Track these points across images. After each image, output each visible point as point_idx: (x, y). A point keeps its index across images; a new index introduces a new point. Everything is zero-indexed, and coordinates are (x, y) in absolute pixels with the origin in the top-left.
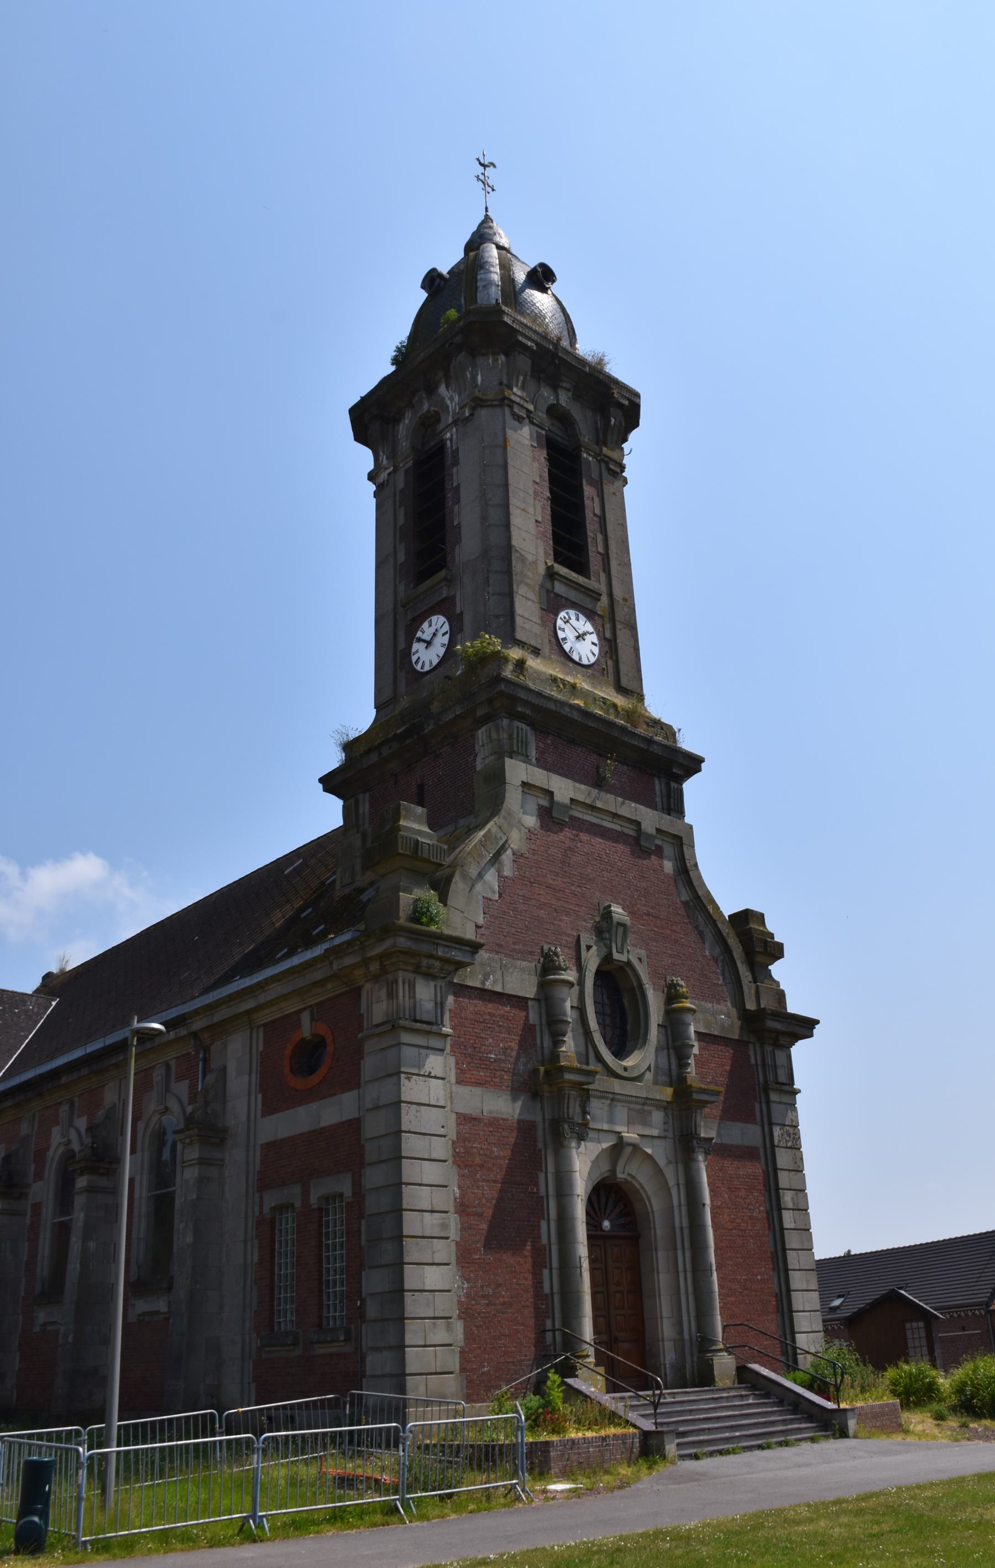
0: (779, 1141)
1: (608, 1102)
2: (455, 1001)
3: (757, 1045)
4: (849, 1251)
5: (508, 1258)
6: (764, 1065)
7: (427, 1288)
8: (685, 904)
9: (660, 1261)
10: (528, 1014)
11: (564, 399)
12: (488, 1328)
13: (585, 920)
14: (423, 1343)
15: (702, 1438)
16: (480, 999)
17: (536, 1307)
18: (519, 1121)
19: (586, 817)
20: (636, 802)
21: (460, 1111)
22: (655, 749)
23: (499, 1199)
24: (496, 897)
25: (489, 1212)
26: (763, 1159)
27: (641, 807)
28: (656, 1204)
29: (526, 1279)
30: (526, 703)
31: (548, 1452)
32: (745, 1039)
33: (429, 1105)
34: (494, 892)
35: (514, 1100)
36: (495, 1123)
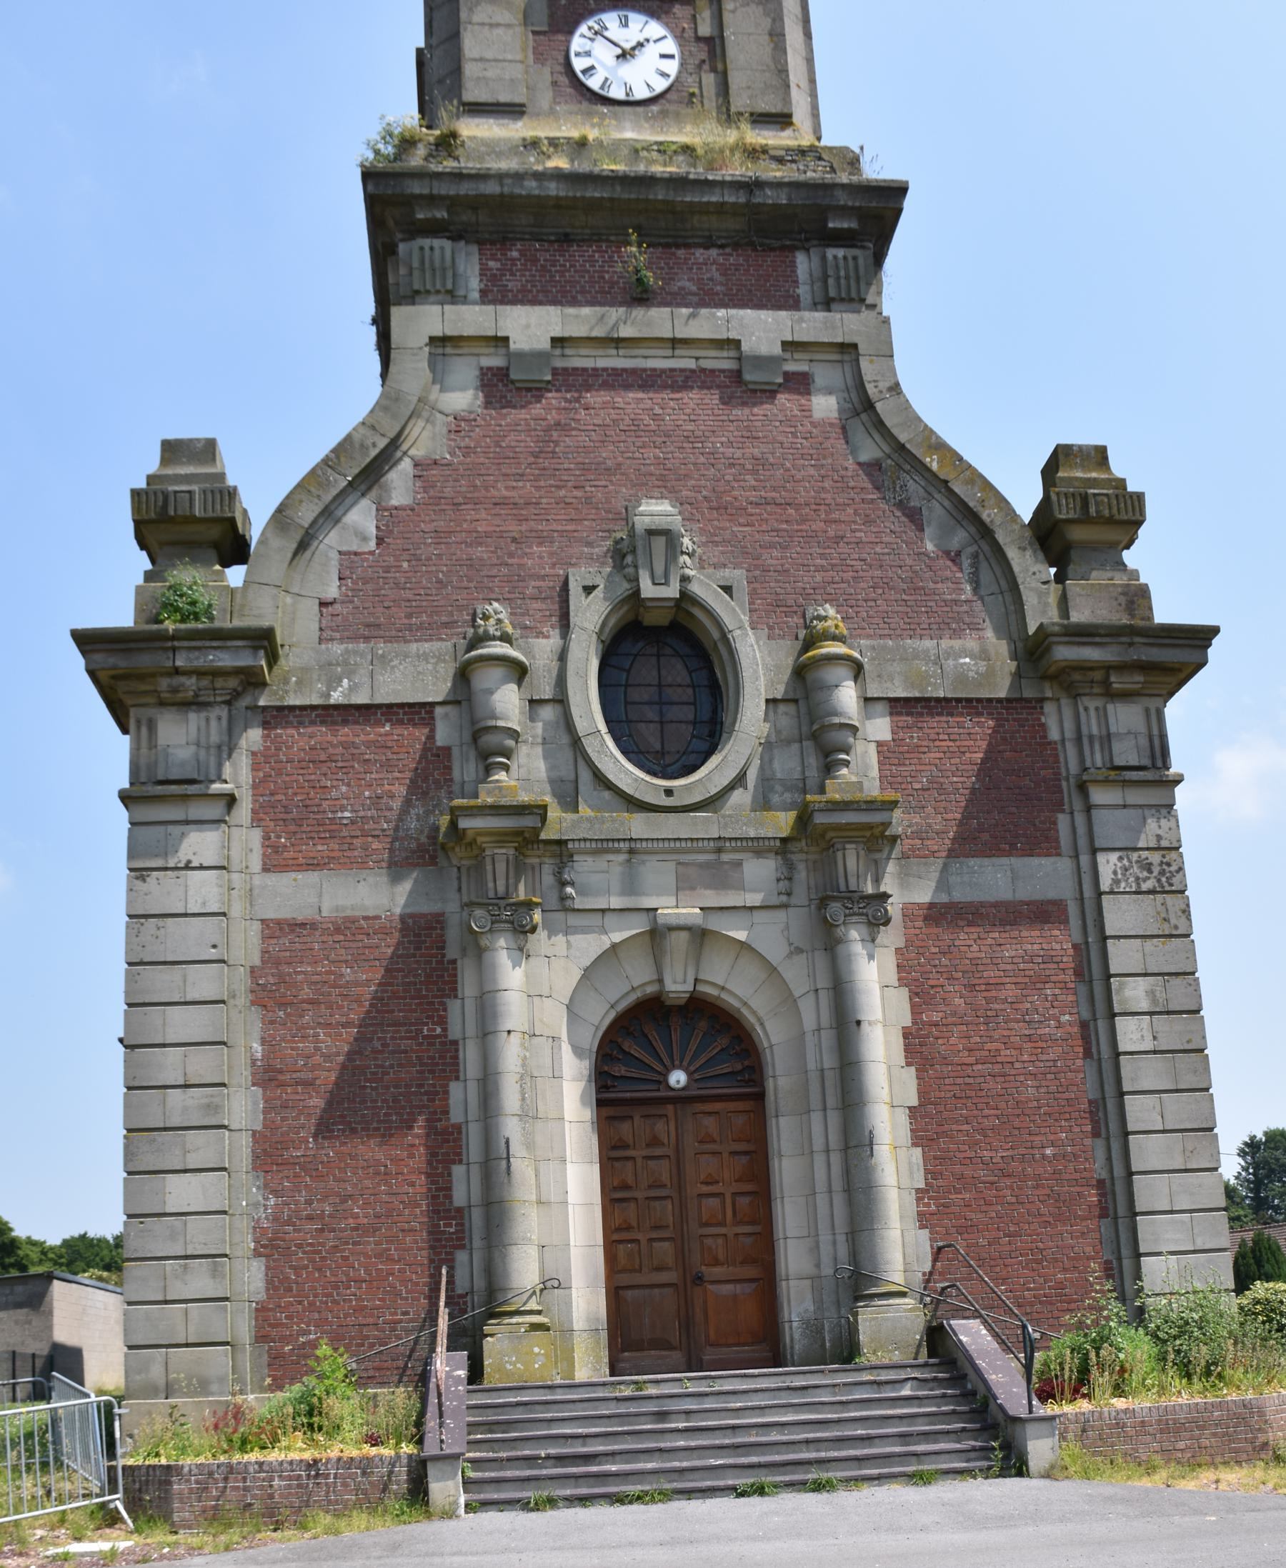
0: (1116, 882)
1: (622, 857)
2: (265, 737)
3: (1065, 702)
5: (371, 1150)
6: (1079, 739)
7: (168, 1210)
8: (872, 468)
9: (784, 1136)
10: (433, 731)
12: (320, 1270)
13: (589, 544)
14: (161, 1298)
15: (677, 1464)
16: (323, 723)
18: (403, 918)
19: (601, 363)
20: (726, 306)
21: (270, 915)
22: (769, 197)
24: (372, 545)
25: (329, 1077)
26: (1075, 922)
27: (741, 312)
28: (773, 1034)
29: (412, 1184)
30: (432, 200)
31: (169, 1483)
32: (1028, 693)
33: (186, 915)
34: (365, 539)
35: (396, 879)
36: (346, 927)
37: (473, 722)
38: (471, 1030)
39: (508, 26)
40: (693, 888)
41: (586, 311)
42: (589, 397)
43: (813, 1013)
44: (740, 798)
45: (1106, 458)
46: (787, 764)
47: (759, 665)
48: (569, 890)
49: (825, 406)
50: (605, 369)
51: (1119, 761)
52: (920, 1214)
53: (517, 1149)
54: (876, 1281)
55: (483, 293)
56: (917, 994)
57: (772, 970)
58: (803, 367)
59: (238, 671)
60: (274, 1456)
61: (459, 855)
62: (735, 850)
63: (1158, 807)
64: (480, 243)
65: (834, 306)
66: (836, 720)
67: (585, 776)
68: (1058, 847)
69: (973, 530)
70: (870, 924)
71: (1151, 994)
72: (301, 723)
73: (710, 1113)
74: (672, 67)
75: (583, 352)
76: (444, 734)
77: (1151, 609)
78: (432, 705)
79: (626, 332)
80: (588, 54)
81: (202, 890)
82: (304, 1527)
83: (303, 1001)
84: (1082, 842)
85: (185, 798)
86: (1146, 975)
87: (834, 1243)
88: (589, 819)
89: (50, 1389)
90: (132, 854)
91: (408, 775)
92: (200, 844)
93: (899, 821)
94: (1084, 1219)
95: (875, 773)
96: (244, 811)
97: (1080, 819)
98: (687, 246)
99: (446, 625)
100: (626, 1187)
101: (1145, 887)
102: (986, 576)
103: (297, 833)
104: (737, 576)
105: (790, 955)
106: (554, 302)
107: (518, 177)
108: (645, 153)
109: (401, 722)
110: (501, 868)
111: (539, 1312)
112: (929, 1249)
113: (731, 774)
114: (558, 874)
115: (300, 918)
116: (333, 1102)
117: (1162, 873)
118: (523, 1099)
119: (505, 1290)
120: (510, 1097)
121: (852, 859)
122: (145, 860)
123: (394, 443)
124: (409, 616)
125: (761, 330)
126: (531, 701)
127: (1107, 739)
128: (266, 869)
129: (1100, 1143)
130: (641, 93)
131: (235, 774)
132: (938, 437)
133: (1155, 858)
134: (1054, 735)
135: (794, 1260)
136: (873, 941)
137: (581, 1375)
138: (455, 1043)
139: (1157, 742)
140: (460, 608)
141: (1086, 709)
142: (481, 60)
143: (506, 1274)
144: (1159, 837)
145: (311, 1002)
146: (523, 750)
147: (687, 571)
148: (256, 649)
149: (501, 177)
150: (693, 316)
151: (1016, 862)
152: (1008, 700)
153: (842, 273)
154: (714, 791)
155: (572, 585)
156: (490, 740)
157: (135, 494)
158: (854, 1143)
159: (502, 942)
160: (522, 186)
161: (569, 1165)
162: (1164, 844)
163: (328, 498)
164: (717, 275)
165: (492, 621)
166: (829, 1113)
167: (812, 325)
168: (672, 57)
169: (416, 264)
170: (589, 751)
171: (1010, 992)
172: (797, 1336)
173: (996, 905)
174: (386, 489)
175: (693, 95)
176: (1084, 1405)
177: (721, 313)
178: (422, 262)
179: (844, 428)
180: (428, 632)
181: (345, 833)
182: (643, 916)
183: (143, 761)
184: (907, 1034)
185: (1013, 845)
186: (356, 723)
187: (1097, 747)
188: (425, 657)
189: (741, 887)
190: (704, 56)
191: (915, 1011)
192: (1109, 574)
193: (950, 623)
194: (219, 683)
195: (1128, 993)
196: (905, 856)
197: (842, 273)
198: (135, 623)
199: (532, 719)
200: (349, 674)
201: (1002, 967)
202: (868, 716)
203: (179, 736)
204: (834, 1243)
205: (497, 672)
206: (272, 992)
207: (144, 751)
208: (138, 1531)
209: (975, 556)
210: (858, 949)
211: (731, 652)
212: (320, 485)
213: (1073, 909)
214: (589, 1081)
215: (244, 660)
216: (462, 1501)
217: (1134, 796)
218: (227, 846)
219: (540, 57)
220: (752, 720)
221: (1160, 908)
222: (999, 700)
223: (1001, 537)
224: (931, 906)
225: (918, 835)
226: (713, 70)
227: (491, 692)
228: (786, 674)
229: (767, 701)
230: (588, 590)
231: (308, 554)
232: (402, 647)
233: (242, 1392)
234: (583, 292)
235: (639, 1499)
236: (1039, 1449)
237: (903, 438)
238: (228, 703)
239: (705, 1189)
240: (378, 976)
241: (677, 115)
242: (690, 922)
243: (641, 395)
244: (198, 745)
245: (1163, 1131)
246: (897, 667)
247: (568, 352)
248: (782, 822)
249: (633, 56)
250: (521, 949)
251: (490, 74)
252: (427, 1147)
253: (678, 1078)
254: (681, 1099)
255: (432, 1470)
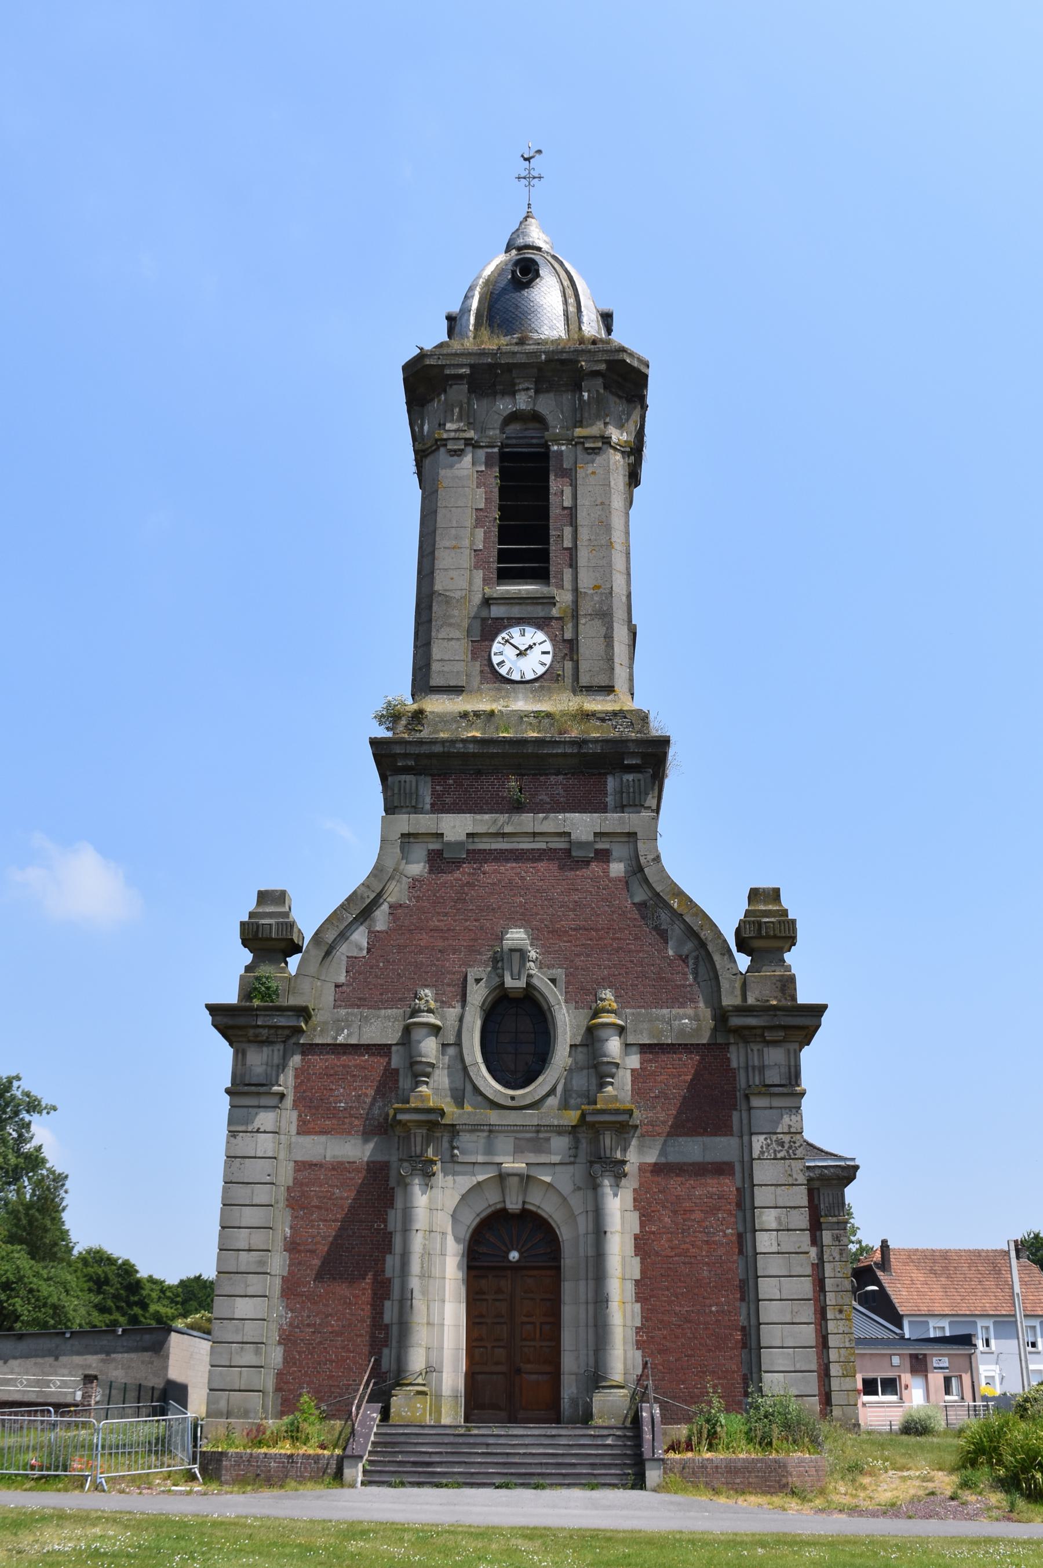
1: (486, 1134)
2: (303, 1060)
3: (741, 1045)
4: (200, 1276)
5: (342, 1289)
8: (641, 906)
10: (390, 1059)
11: (523, 402)
17: (373, 1336)
18: (368, 1163)
19: (494, 846)
21: (299, 1159)
22: (591, 748)
23: (336, 1237)
24: (365, 952)
26: (738, 1175)
27: (573, 815)
28: (565, 1233)
29: (363, 1310)
30: (406, 756)
31: (221, 1461)
33: (255, 1157)
34: (361, 949)
35: (366, 1141)
36: (339, 1167)
37: (411, 1057)
39: (458, 639)
40: (522, 1152)
41: (487, 817)
42: (486, 867)
43: (584, 1224)
44: (553, 1101)
45: (779, 896)
46: (580, 1082)
47: (567, 1023)
48: (456, 1151)
49: (617, 869)
50: (496, 850)
51: (768, 1082)
52: (637, 1341)
53: (417, 1294)
54: (605, 1379)
55: (432, 805)
56: (644, 1216)
57: (565, 1199)
58: (606, 846)
59: (289, 1027)
60: (273, 1451)
61: (398, 1130)
62: (547, 1131)
63: (790, 1108)
64: (432, 775)
65: (626, 809)
66: (605, 1059)
67: (469, 1088)
68: (732, 1130)
69: (696, 942)
70: (615, 1176)
71: (778, 1219)
72: (321, 1053)
73: (531, 1276)
74: (548, 659)
75: (484, 840)
76: (396, 1061)
77: (795, 989)
78: (391, 1045)
79: (508, 829)
80: (501, 653)
81: (265, 1144)
82: (282, 1487)
83: (313, 1206)
84: (745, 1129)
85: (258, 1094)
86: (776, 1207)
87: (587, 1355)
88: (469, 1113)
89: (168, 1410)
90: (230, 1123)
91: (376, 1084)
92: (265, 1119)
93: (638, 1117)
94: (732, 1349)
95: (629, 1087)
96: (289, 1102)
97: (745, 1114)
98: (546, 775)
99: (400, 1000)
100: (482, 1316)
101: (779, 1156)
102: (702, 970)
103: (316, 1113)
104: (559, 973)
105: (574, 1191)
106: (470, 811)
107: (453, 742)
108: (525, 719)
109: (373, 1054)
110: (419, 1139)
111: (424, 1385)
112: (641, 1362)
113: (547, 1088)
114: (451, 1142)
115: (315, 1160)
116: (326, 1262)
117: (790, 1147)
118: (422, 1267)
119: (406, 1371)
120: (415, 1267)
121: (608, 1139)
122: (238, 1123)
123: (379, 895)
124: (381, 994)
125: (582, 825)
126: (443, 1045)
127: (762, 1069)
128: (298, 1133)
129: (744, 1304)
130: (530, 676)
131: (286, 1080)
132: (679, 888)
133: (787, 1138)
134: (734, 1064)
135: (569, 1363)
136: (618, 1186)
137: (445, 1420)
138: (391, 1233)
139: (793, 1070)
140: (409, 990)
141: (752, 1050)
142: (442, 660)
143: (406, 1364)
144: (790, 1126)
145: (317, 1207)
146: (437, 1072)
147: (532, 972)
148: (299, 1016)
149: (443, 742)
150: (545, 818)
151: (707, 1139)
152: (709, 1044)
153: (631, 790)
154: (537, 1098)
155: (469, 978)
156: (418, 1068)
157: (242, 924)
158: (600, 1301)
159: (417, 1181)
160: (455, 747)
161: (447, 1304)
162: (793, 1130)
163: (342, 927)
164: (561, 792)
165: (423, 1002)
166: (590, 1282)
167: (612, 821)
168: (548, 653)
169: (396, 791)
170: (471, 1074)
171: (698, 1215)
172: (566, 1407)
173: (693, 1164)
174: (374, 921)
175: (559, 675)
176: (690, 1455)
177: (560, 816)
178: (400, 790)
179: (627, 882)
180: (392, 1003)
181: (341, 1115)
182: (495, 1167)
183: (238, 1072)
184: (636, 1238)
185: (705, 1130)
186: (350, 1054)
187: (757, 1073)
188: (387, 1018)
189: (549, 1152)
190: (566, 651)
191: (642, 1225)
192: (773, 968)
193: (679, 998)
194: (280, 1032)
195: (764, 1218)
196: (643, 1136)
197: (631, 790)
198: (240, 999)
199: (443, 1055)
200: (348, 1027)
201: (694, 1200)
202: (627, 1054)
203: (258, 1059)
204: (587, 1355)
205: (424, 1031)
206: (298, 1200)
207: (239, 1066)
208: (204, 1484)
209: (697, 958)
210: (608, 1190)
211: (553, 1017)
212: (338, 919)
213: (738, 1167)
214: (463, 1256)
215: (292, 1022)
216: (360, 1479)
217: (777, 1102)
218: (278, 1121)
219: (474, 658)
220: (561, 1056)
221: (787, 1168)
222: (703, 1045)
223: (710, 948)
224: (656, 1164)
225: (651, 1123)
226: (572, 659)
227: (420, 1042)
228: (583, 1031)
229: (571, 1046)
230: (478, 981)
231: (331, 957)
232: (377, 1012)
233: (266, 1418)
234: (487, 803)
235: (446, 1486)
236: (653, 1475)
237: (658, 889)
238: (284, 1042)
239: (525, 1319)
240: (353, 1195)
241: (549, 688)
242: (519, 1172)
243: (514, 865)
244: (267, 1064)
245: (781, 1300)
246: (646, 1025)
247: (476, 840)
248: (572, 1117)
249: (526, 655)
250: (427, 1185)
251: (445, 669)
252: (373, 1290)
253: (514, 1255)
254: (515, 1267)
255: (346, 1463)
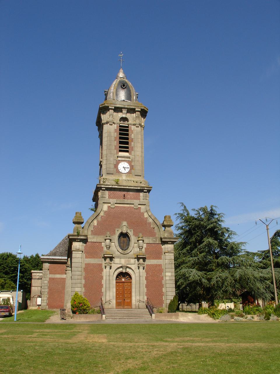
38: (105, 283)
84: (164, 258)
97: (164, 256)
191: (147, 275)
